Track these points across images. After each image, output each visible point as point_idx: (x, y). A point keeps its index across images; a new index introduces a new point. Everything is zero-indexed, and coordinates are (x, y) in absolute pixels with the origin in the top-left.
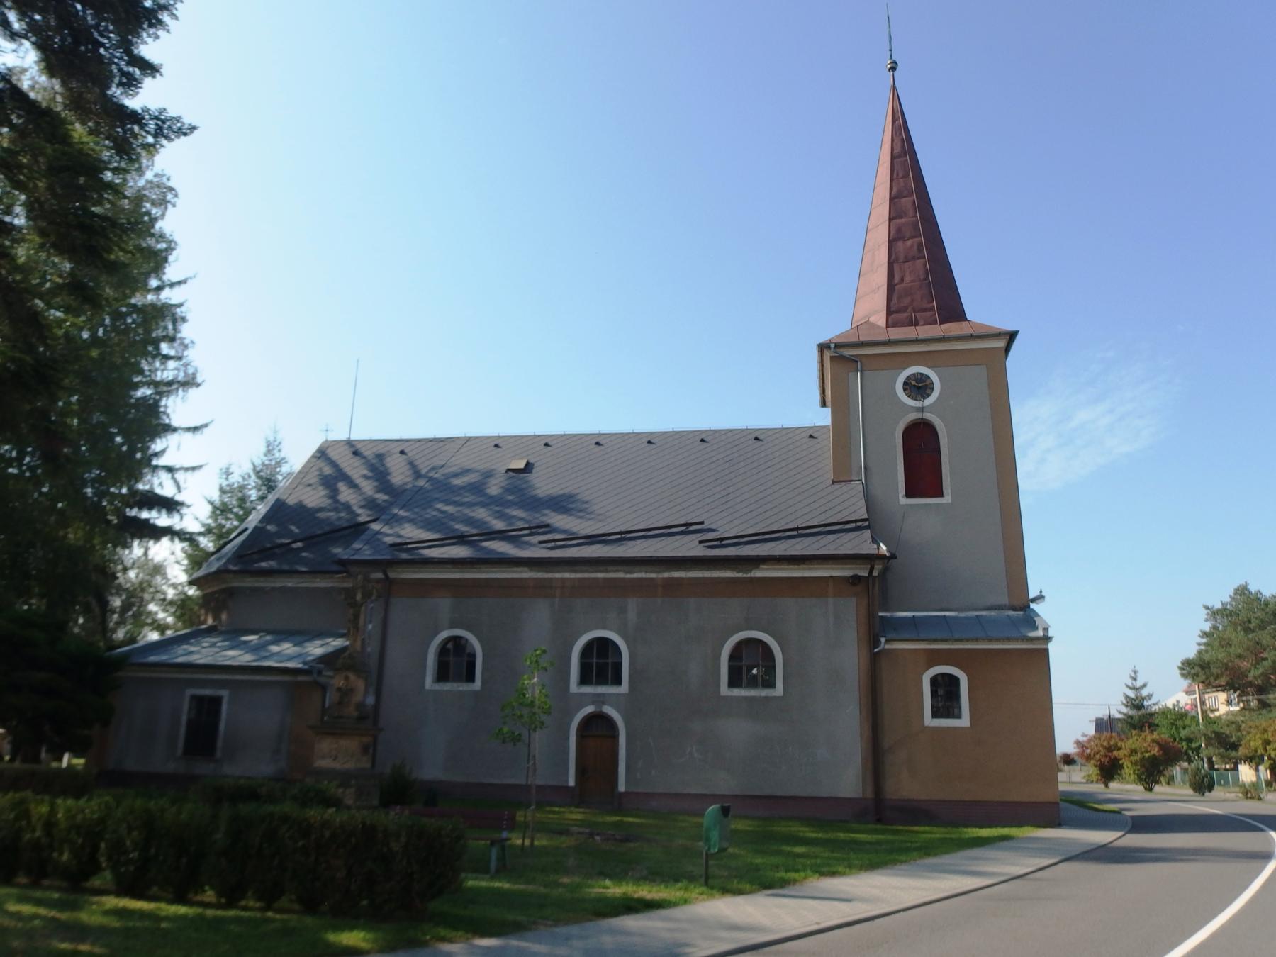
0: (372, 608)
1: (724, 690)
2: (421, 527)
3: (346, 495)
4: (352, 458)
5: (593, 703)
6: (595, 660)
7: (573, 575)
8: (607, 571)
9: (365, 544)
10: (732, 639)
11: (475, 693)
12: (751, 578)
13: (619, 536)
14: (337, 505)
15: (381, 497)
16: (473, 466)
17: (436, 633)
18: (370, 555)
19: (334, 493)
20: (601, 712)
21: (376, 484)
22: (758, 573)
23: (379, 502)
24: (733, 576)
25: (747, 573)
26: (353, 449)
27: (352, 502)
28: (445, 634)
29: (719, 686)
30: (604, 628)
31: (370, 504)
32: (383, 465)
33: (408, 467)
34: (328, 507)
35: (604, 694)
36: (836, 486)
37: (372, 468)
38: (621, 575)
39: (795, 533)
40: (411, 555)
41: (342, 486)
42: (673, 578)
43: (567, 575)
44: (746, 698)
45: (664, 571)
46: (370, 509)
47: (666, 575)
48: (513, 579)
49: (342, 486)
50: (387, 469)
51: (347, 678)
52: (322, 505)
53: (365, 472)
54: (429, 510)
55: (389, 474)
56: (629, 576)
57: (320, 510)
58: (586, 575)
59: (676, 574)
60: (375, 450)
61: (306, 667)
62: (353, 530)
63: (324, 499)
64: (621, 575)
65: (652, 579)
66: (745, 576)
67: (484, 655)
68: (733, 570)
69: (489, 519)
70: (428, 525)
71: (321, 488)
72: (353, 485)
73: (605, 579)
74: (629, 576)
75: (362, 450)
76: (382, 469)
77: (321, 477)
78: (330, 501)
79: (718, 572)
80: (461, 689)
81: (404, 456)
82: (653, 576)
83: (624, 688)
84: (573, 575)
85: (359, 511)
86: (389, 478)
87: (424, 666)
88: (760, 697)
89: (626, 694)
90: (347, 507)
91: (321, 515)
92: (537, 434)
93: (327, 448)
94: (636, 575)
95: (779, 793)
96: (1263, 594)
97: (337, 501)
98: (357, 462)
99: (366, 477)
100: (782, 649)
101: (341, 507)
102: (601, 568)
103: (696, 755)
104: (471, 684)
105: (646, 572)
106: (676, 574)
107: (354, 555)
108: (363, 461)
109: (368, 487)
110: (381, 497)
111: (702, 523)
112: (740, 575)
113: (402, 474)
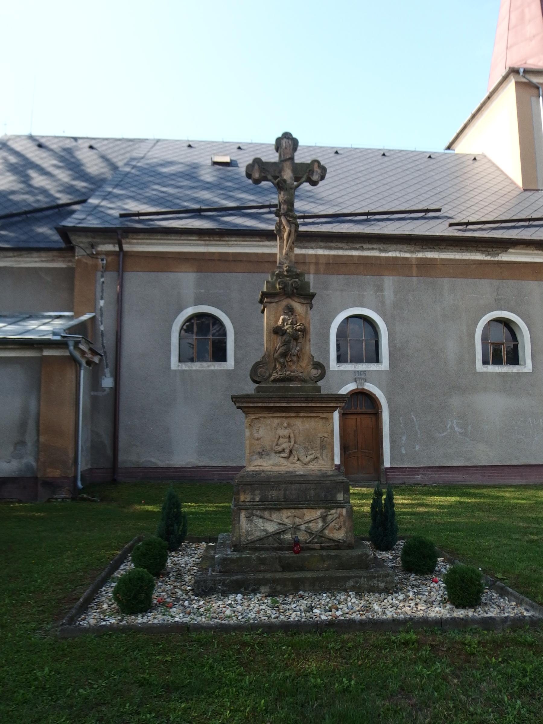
0: (103, 282)
1: (480, 367)
2: (145, 203)
3: (38, 180)
4: (36, 150)
5: (355, 380)
6: (349, 339)
7: (327, 252)
8: (362, 249)
9: (88, 215)
10: (484, 318)
11: (228, 372)
12: (498, 261)
13: (365, 217)
14: (31, 190)
15: (80, 184)
16: (175, 159)
17: (180, 310)
18: (97, 224)
19: (26, 180)
20: (363, 389)
21: (70, 172)
22: (504, 257)
23: (78, 188)
24: (482, 259)
25: (494, 255)
26: (37, 143)
27: (48, 187)
28: (190, 311)
29: (474, 363)
30: (362, 306)
31: (69, 189)
32: (74, 157)
33: (100, 160)
34: (22, 191)
35: (364, 372)
36: (529, 193)
37: (62, 159)
38: (376, 253)
39: (527, 223)
40: (146, 225)
41: (32, 173)
42: (427, 258)
43: (320, 252)
44: (499, 374)
45: (418, 251)
46: (69, 193)
47: (420, 255)
48: (263, 254)
49: (32, 173)
50: (78, 160)
51: (290, 310)
52: (14, 189)
53: (55, 162)
54: (147, 190)
55: (82, 165)
56: (383, 255)
57: (13, 192)
58: (340, 252)
59: (430, 255)
60: (61, 144)
61: (58, 338)
62: (56, 210)
63: (14, 184)
64: (376, 253)
65: (406, 258)
66: (492, 259)
67: (236, 334)
68: (482, 252)
69: (216, 199)
70: (150, 201)
71: (8, 174)
72: (43, 171)
73: (359, 257)
74: (383, 255)
75: (47, 144)
76: (73, 160)
77: (6, 165)
78: (22, 186)
79: (468, 254)
80: (212, 368)
81: (94, 151)
82: (407, 255)
83: (385, 364)
84: (327, 252)
85: (58, 195)
86: (83, 168)
87: (169, 344)
88: (512, 373)
89: (386, 371)
90: (44, 191)
91: (16, 198)
92: (225, 140)
93: (9, 140)
94: (390, 254)
95: (533, 462)
96: (259, 360)
97: (30, 186)
98: (43, 154)
99: (58, 167)
100: (529, 330)
101: (36, 191)
102: (358, 246)
103: (456, 429)
104: (223, 363)
105: (401, 251)
106: (430, 255)
107: (79, 223)
108: (50, 153)
109: (64, 176)
110: (80, 184)
111: (439, 210)
112: (488, 258)
113: (96, 165)
